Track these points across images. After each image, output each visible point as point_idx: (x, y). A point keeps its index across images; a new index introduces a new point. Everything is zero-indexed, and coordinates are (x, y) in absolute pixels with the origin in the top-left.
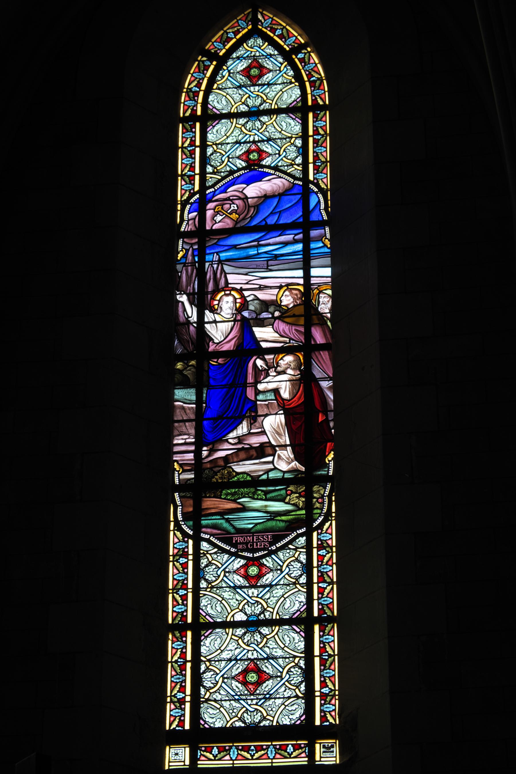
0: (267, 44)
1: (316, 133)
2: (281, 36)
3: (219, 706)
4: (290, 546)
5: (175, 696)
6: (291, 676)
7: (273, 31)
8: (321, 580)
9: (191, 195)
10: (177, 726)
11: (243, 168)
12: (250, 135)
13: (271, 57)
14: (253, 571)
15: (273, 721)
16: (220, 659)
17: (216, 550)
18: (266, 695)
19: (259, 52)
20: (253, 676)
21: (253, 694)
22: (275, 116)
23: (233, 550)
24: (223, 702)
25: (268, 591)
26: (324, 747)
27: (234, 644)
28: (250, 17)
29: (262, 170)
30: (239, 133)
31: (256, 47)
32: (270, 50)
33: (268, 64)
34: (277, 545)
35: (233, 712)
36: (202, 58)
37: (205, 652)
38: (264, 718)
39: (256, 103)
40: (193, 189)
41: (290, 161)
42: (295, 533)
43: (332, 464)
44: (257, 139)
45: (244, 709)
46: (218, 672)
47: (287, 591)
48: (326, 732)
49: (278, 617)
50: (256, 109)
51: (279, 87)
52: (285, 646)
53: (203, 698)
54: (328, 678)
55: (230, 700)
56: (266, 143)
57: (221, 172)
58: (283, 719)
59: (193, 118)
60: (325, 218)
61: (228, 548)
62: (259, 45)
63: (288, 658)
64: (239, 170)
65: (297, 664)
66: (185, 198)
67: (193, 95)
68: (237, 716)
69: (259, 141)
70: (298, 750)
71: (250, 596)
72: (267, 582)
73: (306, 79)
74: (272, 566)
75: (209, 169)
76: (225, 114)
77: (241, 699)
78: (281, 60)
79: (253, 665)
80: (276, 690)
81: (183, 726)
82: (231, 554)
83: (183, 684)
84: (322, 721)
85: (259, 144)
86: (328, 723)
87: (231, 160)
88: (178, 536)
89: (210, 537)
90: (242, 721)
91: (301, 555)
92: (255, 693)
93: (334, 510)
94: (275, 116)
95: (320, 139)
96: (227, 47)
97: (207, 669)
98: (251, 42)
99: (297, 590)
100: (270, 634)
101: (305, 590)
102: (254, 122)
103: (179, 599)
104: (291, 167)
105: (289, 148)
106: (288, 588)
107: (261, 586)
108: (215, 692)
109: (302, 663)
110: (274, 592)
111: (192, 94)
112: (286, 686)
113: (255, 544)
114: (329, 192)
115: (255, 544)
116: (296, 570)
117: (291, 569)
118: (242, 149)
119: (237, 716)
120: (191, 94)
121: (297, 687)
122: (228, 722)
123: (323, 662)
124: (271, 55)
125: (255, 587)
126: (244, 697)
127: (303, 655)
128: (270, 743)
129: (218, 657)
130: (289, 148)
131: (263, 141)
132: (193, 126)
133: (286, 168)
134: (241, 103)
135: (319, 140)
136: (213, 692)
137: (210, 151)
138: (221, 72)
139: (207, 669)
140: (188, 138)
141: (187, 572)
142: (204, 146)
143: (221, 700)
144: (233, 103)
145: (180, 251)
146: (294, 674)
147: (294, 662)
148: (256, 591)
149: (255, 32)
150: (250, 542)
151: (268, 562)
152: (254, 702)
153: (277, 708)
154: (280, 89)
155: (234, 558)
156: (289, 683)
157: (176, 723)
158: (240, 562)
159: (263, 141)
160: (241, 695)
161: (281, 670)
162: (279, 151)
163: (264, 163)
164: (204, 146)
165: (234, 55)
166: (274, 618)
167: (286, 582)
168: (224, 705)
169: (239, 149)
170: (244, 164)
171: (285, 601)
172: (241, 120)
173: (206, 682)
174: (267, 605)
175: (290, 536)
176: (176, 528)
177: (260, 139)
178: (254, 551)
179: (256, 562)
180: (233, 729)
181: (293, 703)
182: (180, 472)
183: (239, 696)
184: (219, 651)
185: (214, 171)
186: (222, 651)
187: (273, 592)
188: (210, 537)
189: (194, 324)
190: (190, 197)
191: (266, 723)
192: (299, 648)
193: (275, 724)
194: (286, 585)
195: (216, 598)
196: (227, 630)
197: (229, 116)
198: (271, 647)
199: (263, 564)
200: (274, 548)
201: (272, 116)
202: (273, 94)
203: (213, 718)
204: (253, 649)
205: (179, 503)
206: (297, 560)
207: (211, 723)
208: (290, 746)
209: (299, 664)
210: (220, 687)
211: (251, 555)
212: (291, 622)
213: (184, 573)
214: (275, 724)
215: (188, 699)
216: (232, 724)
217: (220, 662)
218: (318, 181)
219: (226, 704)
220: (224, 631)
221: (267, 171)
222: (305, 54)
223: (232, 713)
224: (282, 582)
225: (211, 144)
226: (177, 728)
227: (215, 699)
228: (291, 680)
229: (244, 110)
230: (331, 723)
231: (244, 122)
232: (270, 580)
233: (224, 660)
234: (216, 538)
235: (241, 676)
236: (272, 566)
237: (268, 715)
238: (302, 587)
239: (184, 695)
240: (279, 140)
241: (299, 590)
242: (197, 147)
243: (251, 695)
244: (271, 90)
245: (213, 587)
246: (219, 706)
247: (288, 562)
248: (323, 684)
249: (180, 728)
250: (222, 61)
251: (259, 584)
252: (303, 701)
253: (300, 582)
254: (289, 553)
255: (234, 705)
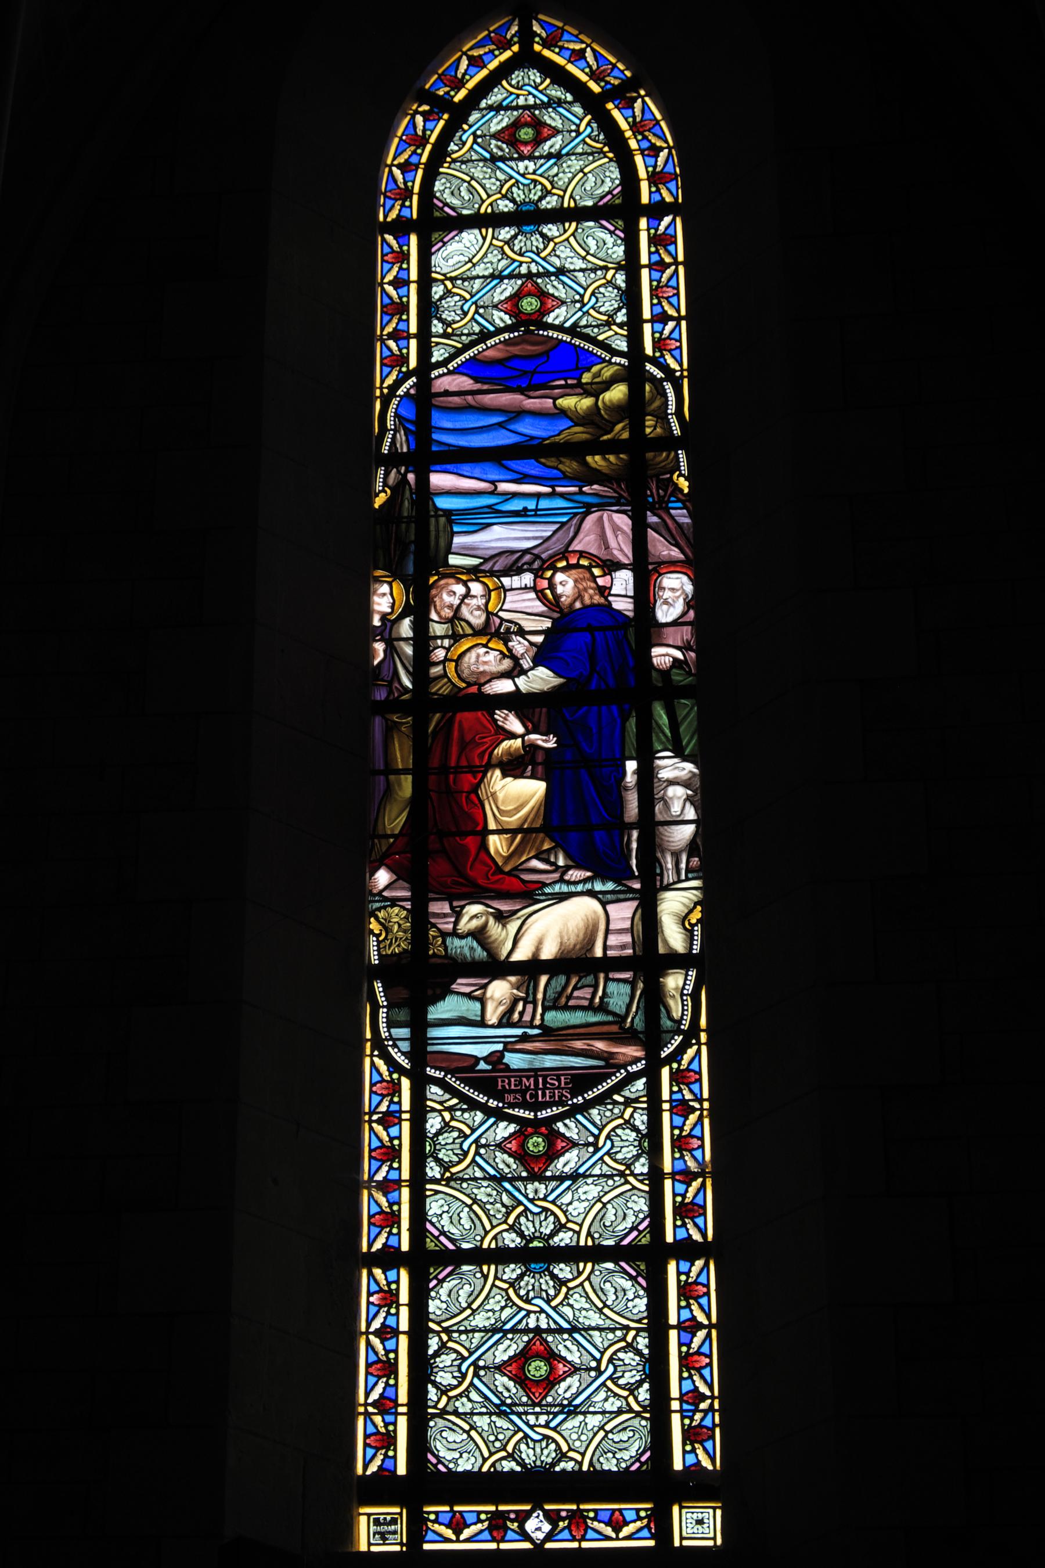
0: (548, 81)
4: (616, 1097)
6: (619, 1369)
11: (508, 329)
12: (521, 263)
13: (560, 106)
14: (536, 1144)
16: (469, 1328)
19: (534, 96)
21: (539, 1405)
23: (493, 1103)
24: (475, 1418)
25: (568, 1188)
29: (546, 333)
30: (500, 257)
31: (528, 87)
33: (552, 119)
35: (497, 1439)
36: (419, 106)
38: (562, 1456)
39: (531, 196)
41: (605, 318)
42: (622, 1071)
45: (520, 1435)
49: (590, 1243)
52: (607, 1433)
54: (697, 1379)
55: (490, 1414)
56: (553, 278)
57: (462, 334)
60: (677, 431)
61: (482, 1099)
62: (534, 81)
64: (499, 331)
68: (504, 1449)
69: (539, 275)
75: (437, 327)
77: (513, 1413)
78: (578, 110)
80: (588, 1397)
82: (488, 1112)
85: (539, 281)
89: (445, 1076)
91: (639, 1339)
93: (703, 1022)
98: (517, 76)
99: (628, 1187)
101: (625, 333)
102: (538, 1463)
104: (606, 328)
106: (610, 1182)
108: (460, 1395)
109: (642, 1342)
113: (540, 1092)
115: (540, 1092)
116: (627, 1143)
117: (616, 1144)
118: (502, 120)
122: (485, 1460)
125: (542, 1179)
126: (521, 1409)
129: (466, 1323)
130: (602, 290)
131: (547, 274)
133: (596, 330)
134: (499, 196)
136: (456, 1396)
137: (437, 291)
138: (458, 134)
142: (426, 281)
144: (484, 196)
145: (380, 492)
146: (625, 1365)
148: (543, 1186)
149: (527, 59)
150: (528, 1088)
151: (569, 1129)
153: (591, 1434)
154: (578, 168)
155: (492, 1120)
156: (611, 1158)
160: (516, 1405)
161: (598, 1355)
162: (582, 296)
163: (550, 319)
164: (426, 281)
165: (483, 104)
166: (582, 1243)
168: (478, 1424)
171: (604, 1210)
173: (634, 1363)
174: (566, 1217)
176: (376, 1053)
178: (536, 1107)
179: (547, 1128)
180: (495, 1476)
181: (625, 1425)
182: (381, 939)
185: (445, 331)
187: (580, 1190)
188: (445, 1076)
189: (402, 471)
190: (398, 384)
191: (569, 1466)
192: (614, 256)
196: (485, 1268)
198: (577, 1306)
203: (455, 1450)
205: (382, 1000)
206: (629, 1124)
207: (450, 1461)
209: (635, 1344)
210: (468, 1387)
211: (532, 1116)
214: (585, 1468)
216: (493, 1465)
217: (470, 1335)
219: (482, 1422)
220: (478, 1269)
223: (493, 1442)
224: (596, 1171)
225: (442, 277)
228: (619, 1378)
231: (508, 236)
233: (480, 1331)
234: (457, 1079)
236: (497, 1153)
238: (641, 1181)
240: (581, 274)
241: (634, 1188)
243: (534, 1405)
244: (561, 170)
250: (459, 115)
251: (548, 1174)
254: (611, 1110)
255: (498, 1425)
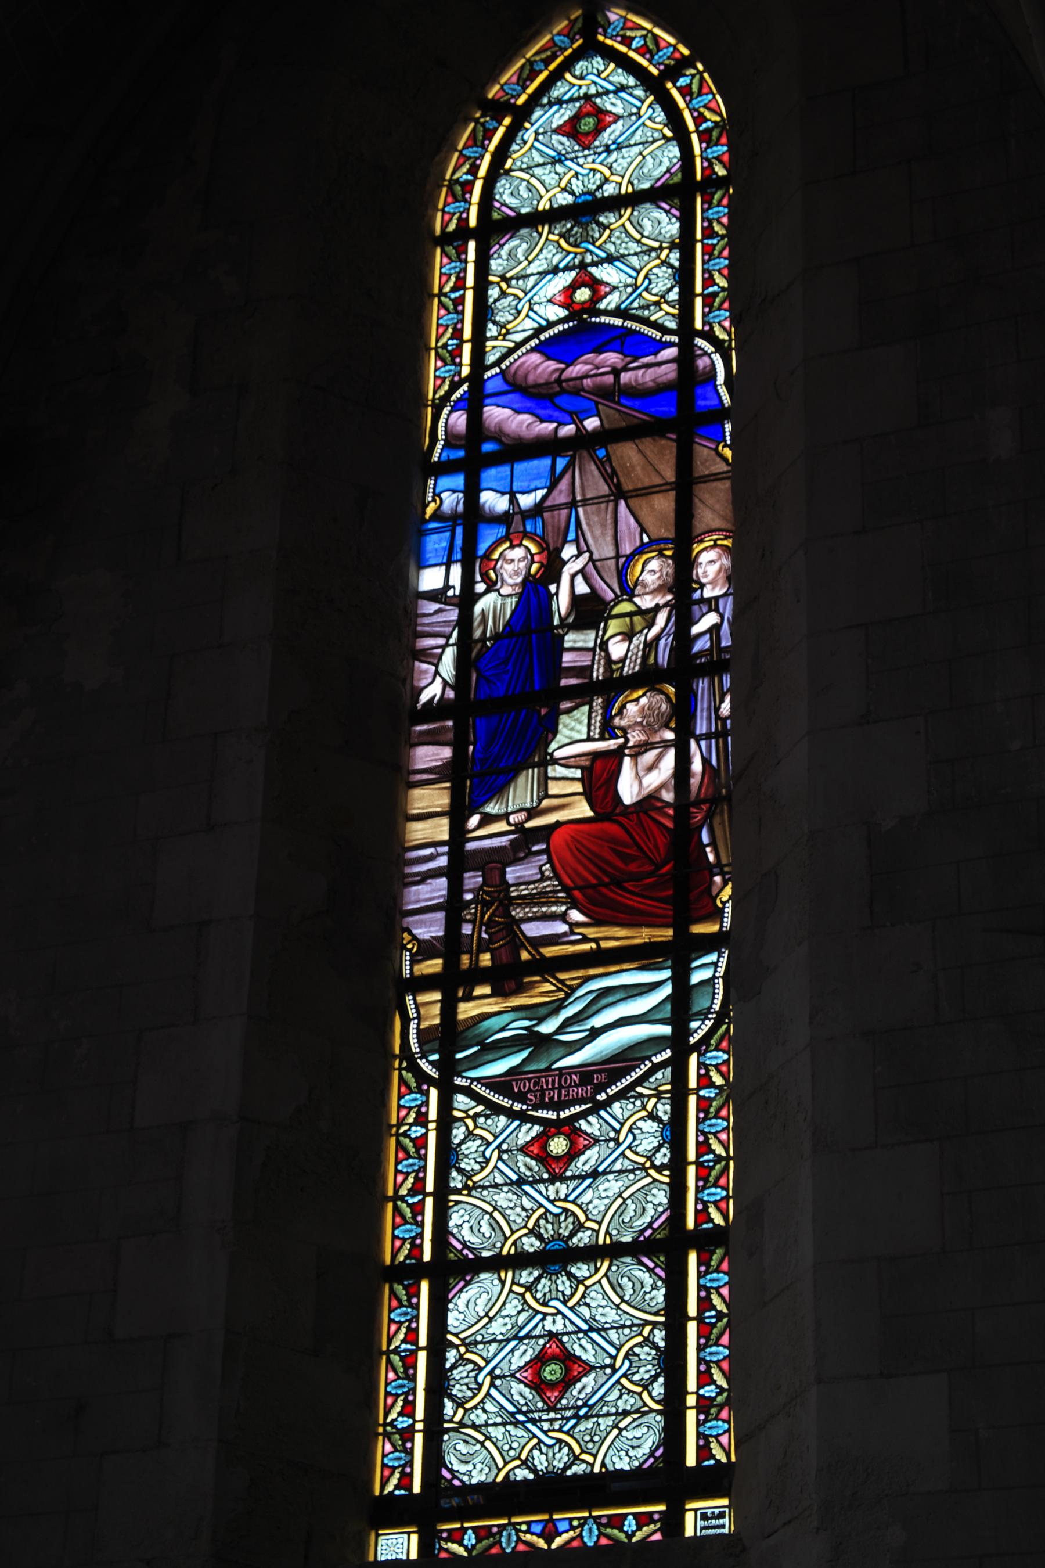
1: (704, 1081)
2: (642, 51)
3: (481, 1438)
5: (392, 1424)
7: (627, 41)
8: (704, 1081)
9: (454, 387)
10: (397, 1487)
11: (562, 321)
15: (592, 1465)
17: (481, 1108)
18: (579, 1408)
20: (555, 1371)
21: (554, 1409)
22: (606, 1264)
23: (517, 1107)
24: (490, 1429)
25: (589, 1186)
26: (704, 1517)
27: (515, 1302)
28: (579, 25)
29: (598, 320)
32: (621, 77)
33: (612, 104)
34: (609, 1090)
37: (456, 1324)
40: (460, 373)
42: (647, 1062)
43: (729, 910)
44: (593, 90)
46: (482, 1363)
47: (627, 1183)
48: (710, 1480)
50: (589, 198)
51: (636, 150)
53: (451, 1421)
55: (504, 1424)
58: (615, 1459)
59: (463, 232)
61: (506, 1103)
63: (632, 1171)
65: (646, 1339)
66: (441, 393)
67: (462, 190)
69: (598, 95)
70: (648, 1525)
71: (552, 1198)
72: (586, 1168)
73: (691, 126)
74: (597, 1133)
76: (527, 214)
78: (639, 92)
79: (554, 1345)
81: (409, 1487)
82: (511, 1114)
83: (411, 1398)
84: (700, 1459)
85: (598, 100)
86: (712, 1462)
87: (498, 1382)
88: (398, 1293)
90: (528, 1468)
92: (559, 1406)
94: (606, 1264)
95: (714, 1099)
96: (530, 91)
97: (461, 1360)
98: (581, 66)
100: (591, 1276)
101: (676, 312)
103: (408, 1213)
105: (655, 271)
107: (573, 1178)
108: (475, 1407)
110: (601, 1188)
111: (459, 188)
112: (623, 1387)
114: (734, 352)
119: (519, 1458)
120: (458, 189)
121: (645, 1388)
123: (703, 1175)
124: (622, 88)
127: (662, 1319)
128: (586, 1514)
131: (607, 92)
132: (456, 353)
134: (525, 1231)
135: (714, 246)
136: (471, 1409)
138: (520, 134)
139: (461, 1360)
140: (450, 275)
141: (423, 1221)
143: (487, 1425)
147: (640, 1334)
149: (592, 48)
151: (591, 1126)
152: (590, 159)
157: (394, 1481)
158: (531, 1128)
159: (607, 92)
167: (643, 302)
168: (493, 1435)
169: (517, 1353)
170: (563, 313)
172: (524, 1273)
175: (638, 1070)
177: (600, 90)
179: (568, 1128)
183: (524, 1414)
184: (486, 1320)
186: (491, 1320)
191: (579, 1469)
193: (597, 1470)
194: (626, 1171)
195: (476, 1323)
197: (498, 1264)
199: (580, 1130)
200: (602, 1097)
201: (622, 212)
202: (602, 1205)
203: (471, 1464)
204: (554, 1311)
207: (464, 1474)
208: (630, 1517)
210: (485, 1397)
212: (636, 1249)
213: (416, 1223)
215: (419, 1426)
218: (712, 328)
219: (497, 1432)
221: (607, 321)
222: (693, 76)
225: (463, 1115)
226: (397, 1492)
227: (474, 1423)
229: (564, 203)
230: (718, 1461)
232: (592, 1162)
234: (483, 1085)
235: (536, 1145)
237: (583, 1452)
239: (411, 1421)
241: (655, 1180)
242: (429, 1194)
245: (508, 332)
246: (481, 1438)
247: (634, 1126)
248: (705, 1379)
249: (403, 1492)
250: (522, 115)
251: (569, 1174)
252: (659, 1418)
253: (670, 299)
255: (513, 1433)
